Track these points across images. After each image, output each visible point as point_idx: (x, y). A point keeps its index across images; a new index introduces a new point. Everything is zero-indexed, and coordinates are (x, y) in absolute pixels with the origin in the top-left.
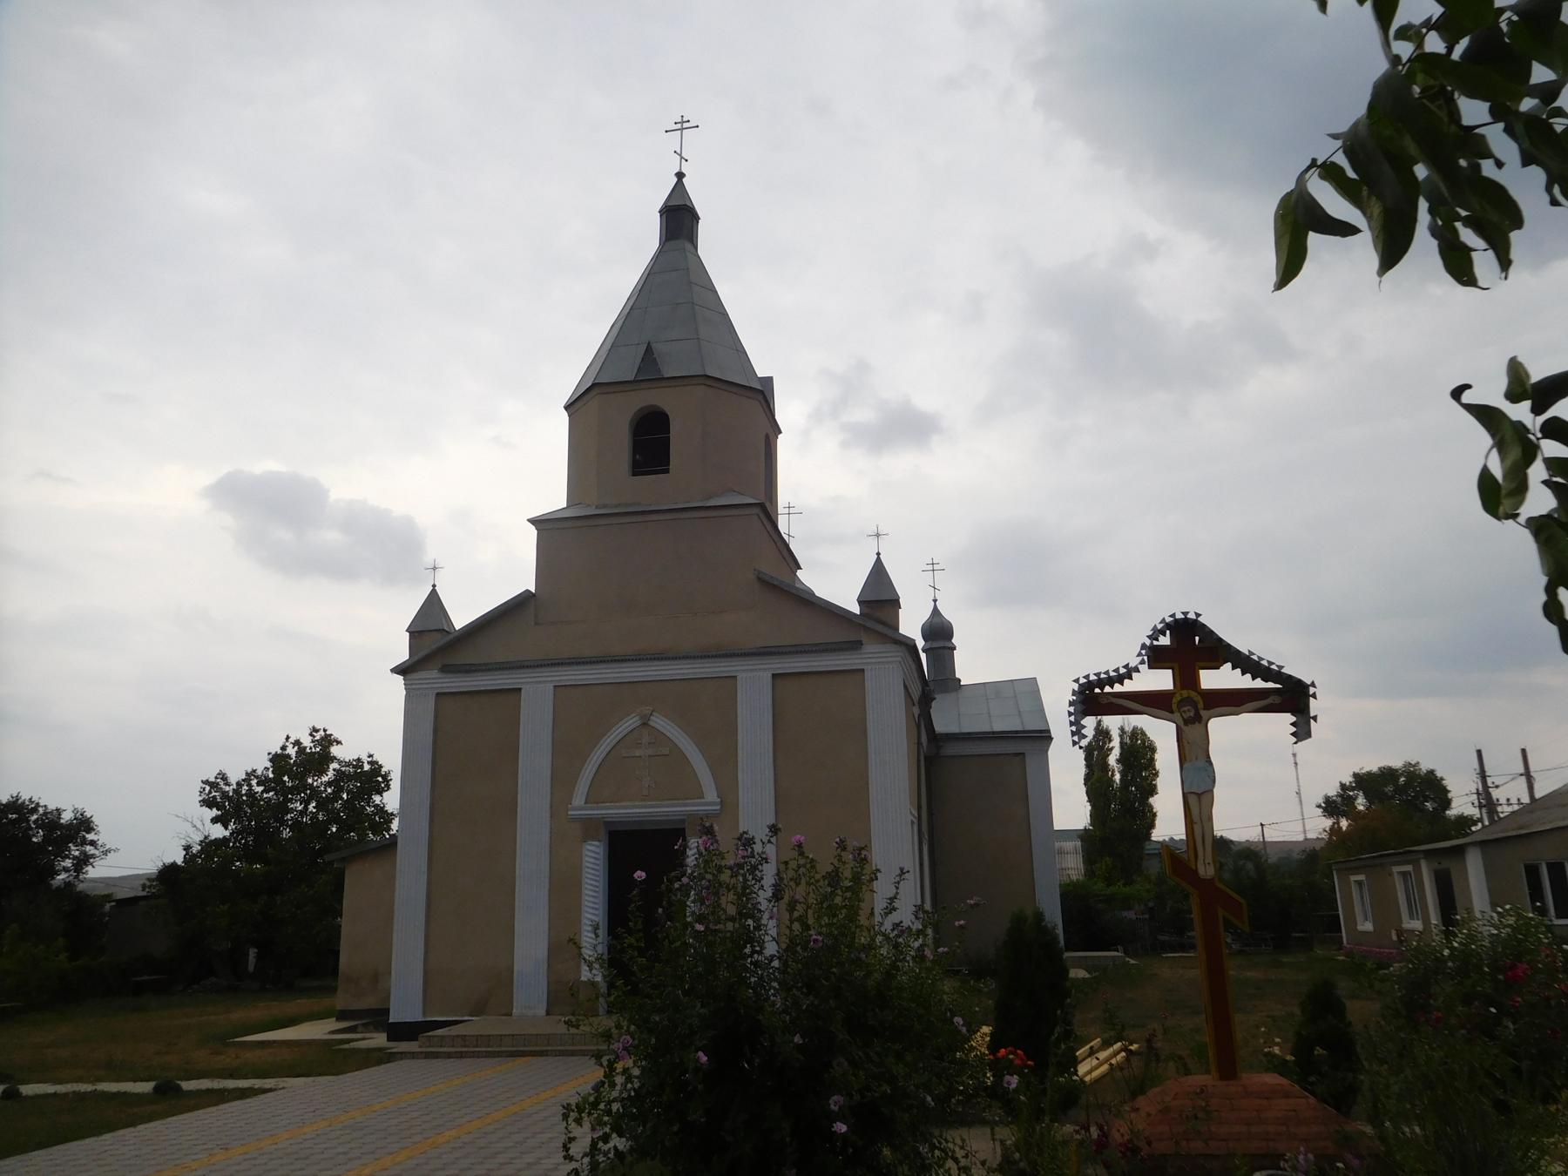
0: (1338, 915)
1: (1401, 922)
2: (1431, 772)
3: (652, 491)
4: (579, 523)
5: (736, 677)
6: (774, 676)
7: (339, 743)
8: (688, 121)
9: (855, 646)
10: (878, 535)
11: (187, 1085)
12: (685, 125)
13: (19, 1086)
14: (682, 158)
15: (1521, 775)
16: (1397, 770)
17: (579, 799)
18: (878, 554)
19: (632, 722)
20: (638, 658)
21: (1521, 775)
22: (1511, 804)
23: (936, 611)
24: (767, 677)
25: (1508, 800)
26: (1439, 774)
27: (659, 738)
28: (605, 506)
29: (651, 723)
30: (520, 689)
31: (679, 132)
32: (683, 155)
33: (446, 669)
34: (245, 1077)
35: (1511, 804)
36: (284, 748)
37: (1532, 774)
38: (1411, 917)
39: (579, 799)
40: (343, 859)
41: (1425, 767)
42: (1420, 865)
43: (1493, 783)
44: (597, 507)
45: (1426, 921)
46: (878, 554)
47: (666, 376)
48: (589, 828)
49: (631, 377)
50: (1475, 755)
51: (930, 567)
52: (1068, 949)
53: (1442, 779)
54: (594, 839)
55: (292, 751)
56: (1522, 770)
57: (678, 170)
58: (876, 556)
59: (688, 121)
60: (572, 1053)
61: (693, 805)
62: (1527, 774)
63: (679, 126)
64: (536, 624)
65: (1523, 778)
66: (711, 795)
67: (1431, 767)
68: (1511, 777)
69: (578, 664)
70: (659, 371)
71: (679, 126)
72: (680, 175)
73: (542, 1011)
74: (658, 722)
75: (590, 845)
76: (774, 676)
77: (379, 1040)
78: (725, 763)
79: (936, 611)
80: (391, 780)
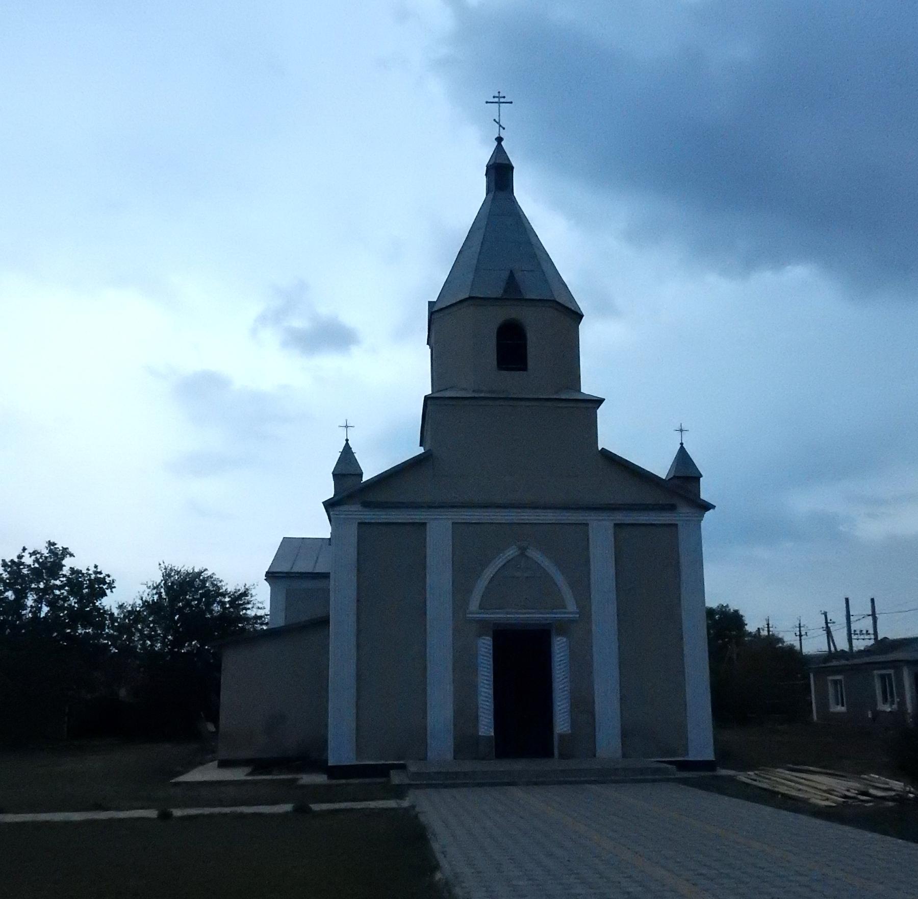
1: (876, 705)
2: (736, 612)
3: (512, 382)
5: (587, 525)
7: (72, 555)
8: (504, 97)
9: (672, 508)
10: (347, 427)
11: (316, 807)
12: (502, 100)
13: (172, 810)
14: (500, 126)
15: (869, 615)
16: (714, 610)
17: (474, 605)
18: (347, 440)
20: (534, 506)
21: (869, 615)
22: (869, 634)
24: (449, 524)
25: (867, 631)
26: (741, 613)
29: (527, 554)
30: (424, 524)
31: (497, 104)
32: (498, 125)
33: (367, 505)
34: (214, 806)
35: (869, 634)
36: (20, 557)
37: (877, 616)
38: (885, 700)
39: (474, 605)
41: (733, 607)
43: (831, 620)
45: (902, 703)
46: (347, 440)
47: (525, 298)
48: (483, 626)
50: (844, 602)
53: (742, 616)
54: (487, 635)
55: (28, 560)
56: (870, 613)
57: (497, 136)
58: (345, 442)
59: (504, 97)
60: (566, 783)
61: (560, 613)
62: (874, 615)
63: (496, 100)
65: (871, 618)
66: (572, 606)
67: (736, 608)
68: (862, 616)
71: (496, 100)
72: (499, 140)
73: (450, 756)
74: (535, 554)
75: (484, 639)
76: (616, 525)
77: (320, 779)
78: (582, 588)
80: (114, 587)
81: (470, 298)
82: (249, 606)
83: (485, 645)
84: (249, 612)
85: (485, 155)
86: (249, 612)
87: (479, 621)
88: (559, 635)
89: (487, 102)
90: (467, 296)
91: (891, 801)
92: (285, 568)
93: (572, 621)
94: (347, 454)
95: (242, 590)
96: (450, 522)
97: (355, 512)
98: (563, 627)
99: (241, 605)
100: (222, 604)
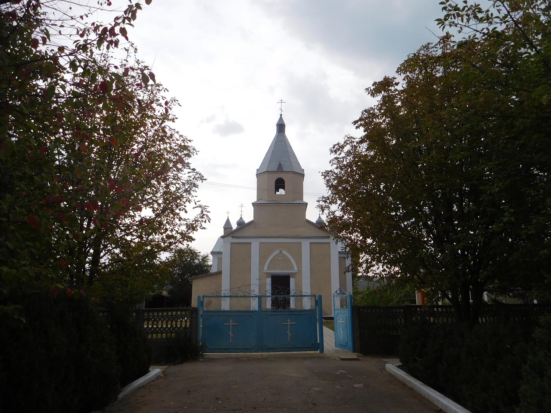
0: (416, 299)
4: (258, 205)
6: (310, 243)
12: (282, 102)
17: (265, 268)
19: (277, 252)
23: (241, 218)
27: (284, 255)
28: (269, 201)
39: (265, 268)
40: (192, 279)
42: (312, 286)
44: (267, 201)
48: (268, 274)
49: (276, 170)
51: (241, 206)
52: (416, 303)
57: (280, 114)
64: (254, 228)
66: (296, 269)
69: (265, 238)
70: (282, 169)
72: (281, 115)
74: (284, 252)
76: (310, 243)
79: (241, 218)
81: (267, 171)
82: (209, 261)
83: (269, 281)
84: (208, 263)
85: (276, 120)
86: (208, 263)
87: (267, 273)
88: (292, 277)
89: (194, 208)
90: (266, 171)
91: (483, 318)
92: (217, 250)
93: (295, 273)
94: (228, 222)
95: (206, 255)
96: (259, 242)
97: (230, 239)
98: (294, 275)
99: (206, 260)
100: (199, 260)
